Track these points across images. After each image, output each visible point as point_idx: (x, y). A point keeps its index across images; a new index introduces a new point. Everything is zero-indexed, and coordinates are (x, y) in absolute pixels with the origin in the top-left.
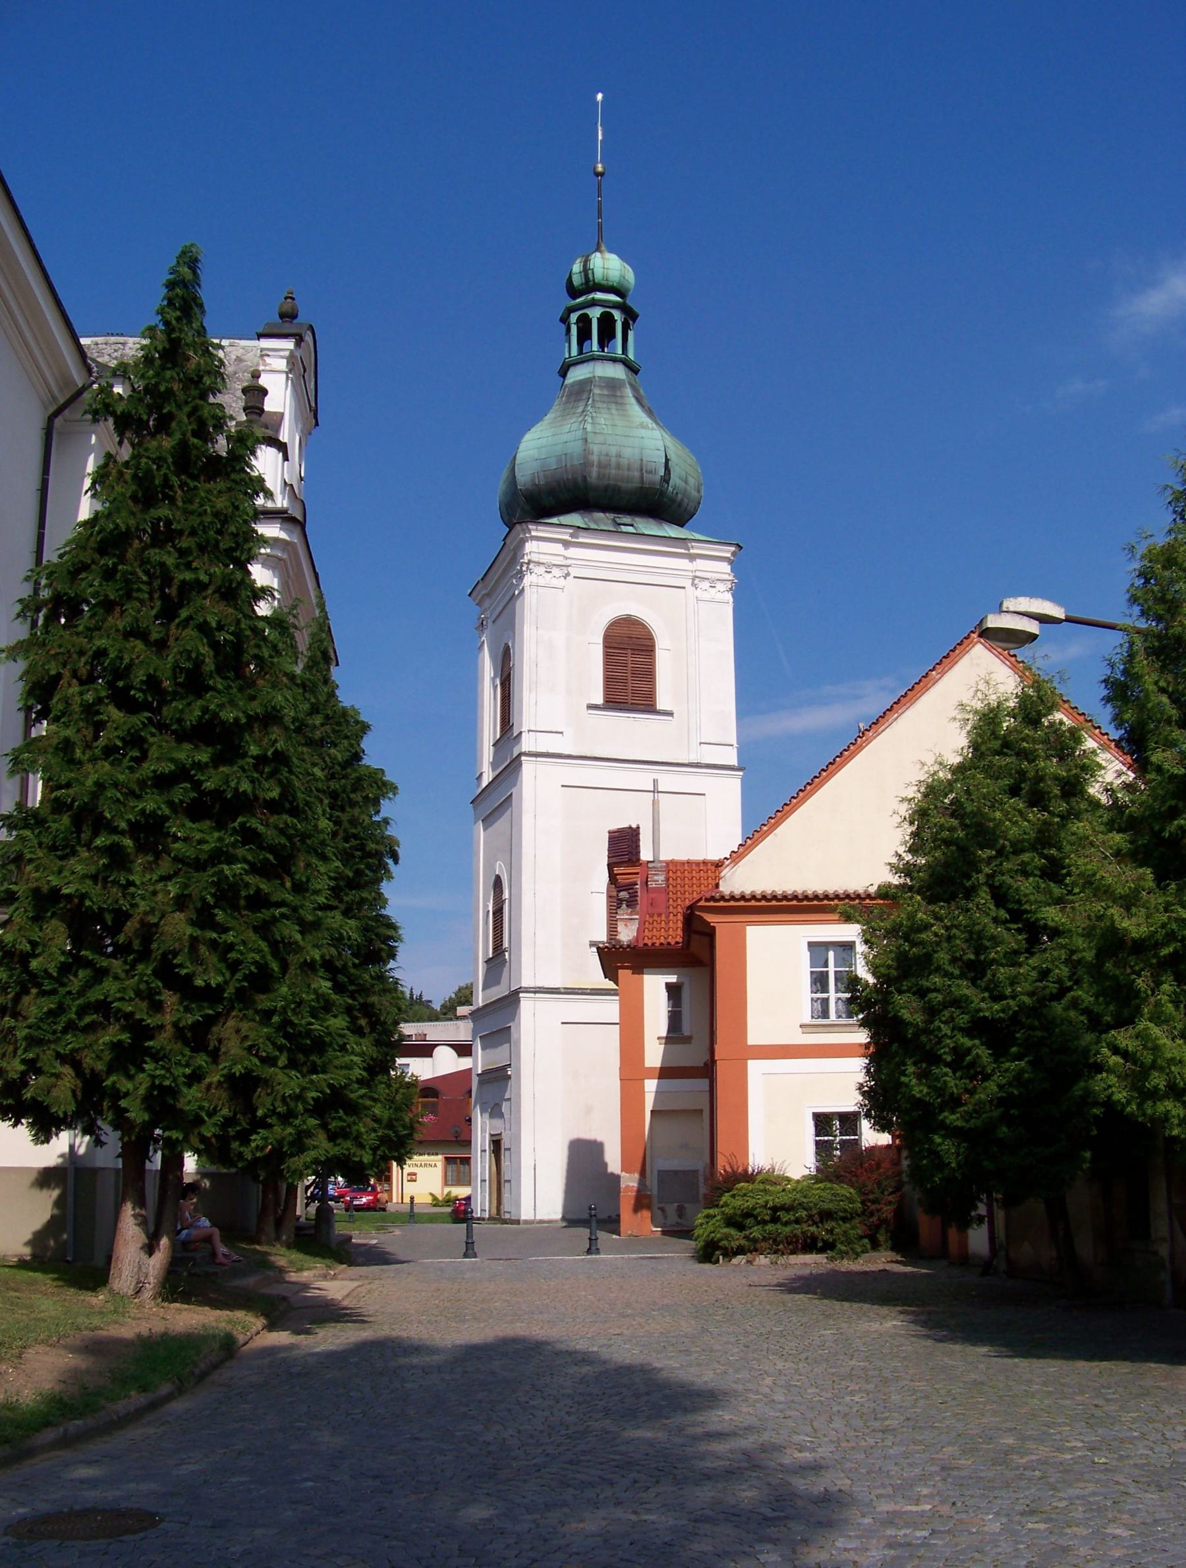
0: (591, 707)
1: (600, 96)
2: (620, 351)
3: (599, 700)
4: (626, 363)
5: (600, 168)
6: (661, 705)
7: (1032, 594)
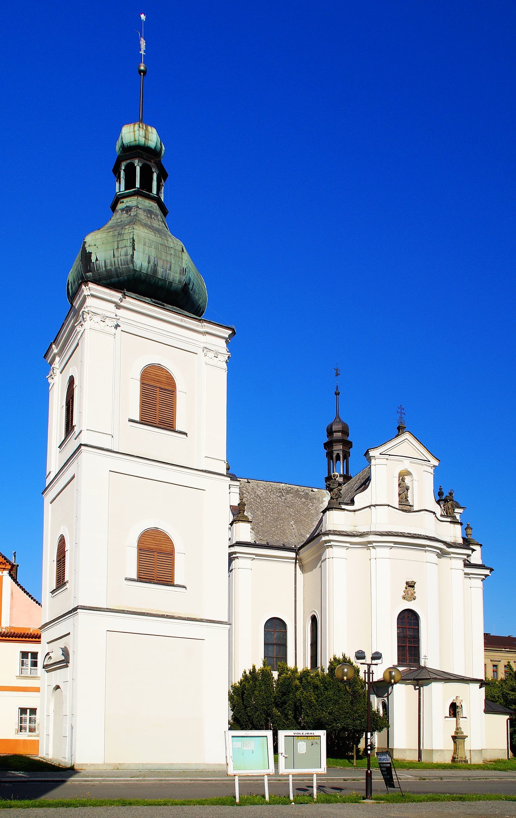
0: (131, 421)
1: (143, 17)
2: (154, 191)
3: (137, 418)
4: (157, 200)
5: (142, 68)
6: (178, 428)
7: (146, 46)
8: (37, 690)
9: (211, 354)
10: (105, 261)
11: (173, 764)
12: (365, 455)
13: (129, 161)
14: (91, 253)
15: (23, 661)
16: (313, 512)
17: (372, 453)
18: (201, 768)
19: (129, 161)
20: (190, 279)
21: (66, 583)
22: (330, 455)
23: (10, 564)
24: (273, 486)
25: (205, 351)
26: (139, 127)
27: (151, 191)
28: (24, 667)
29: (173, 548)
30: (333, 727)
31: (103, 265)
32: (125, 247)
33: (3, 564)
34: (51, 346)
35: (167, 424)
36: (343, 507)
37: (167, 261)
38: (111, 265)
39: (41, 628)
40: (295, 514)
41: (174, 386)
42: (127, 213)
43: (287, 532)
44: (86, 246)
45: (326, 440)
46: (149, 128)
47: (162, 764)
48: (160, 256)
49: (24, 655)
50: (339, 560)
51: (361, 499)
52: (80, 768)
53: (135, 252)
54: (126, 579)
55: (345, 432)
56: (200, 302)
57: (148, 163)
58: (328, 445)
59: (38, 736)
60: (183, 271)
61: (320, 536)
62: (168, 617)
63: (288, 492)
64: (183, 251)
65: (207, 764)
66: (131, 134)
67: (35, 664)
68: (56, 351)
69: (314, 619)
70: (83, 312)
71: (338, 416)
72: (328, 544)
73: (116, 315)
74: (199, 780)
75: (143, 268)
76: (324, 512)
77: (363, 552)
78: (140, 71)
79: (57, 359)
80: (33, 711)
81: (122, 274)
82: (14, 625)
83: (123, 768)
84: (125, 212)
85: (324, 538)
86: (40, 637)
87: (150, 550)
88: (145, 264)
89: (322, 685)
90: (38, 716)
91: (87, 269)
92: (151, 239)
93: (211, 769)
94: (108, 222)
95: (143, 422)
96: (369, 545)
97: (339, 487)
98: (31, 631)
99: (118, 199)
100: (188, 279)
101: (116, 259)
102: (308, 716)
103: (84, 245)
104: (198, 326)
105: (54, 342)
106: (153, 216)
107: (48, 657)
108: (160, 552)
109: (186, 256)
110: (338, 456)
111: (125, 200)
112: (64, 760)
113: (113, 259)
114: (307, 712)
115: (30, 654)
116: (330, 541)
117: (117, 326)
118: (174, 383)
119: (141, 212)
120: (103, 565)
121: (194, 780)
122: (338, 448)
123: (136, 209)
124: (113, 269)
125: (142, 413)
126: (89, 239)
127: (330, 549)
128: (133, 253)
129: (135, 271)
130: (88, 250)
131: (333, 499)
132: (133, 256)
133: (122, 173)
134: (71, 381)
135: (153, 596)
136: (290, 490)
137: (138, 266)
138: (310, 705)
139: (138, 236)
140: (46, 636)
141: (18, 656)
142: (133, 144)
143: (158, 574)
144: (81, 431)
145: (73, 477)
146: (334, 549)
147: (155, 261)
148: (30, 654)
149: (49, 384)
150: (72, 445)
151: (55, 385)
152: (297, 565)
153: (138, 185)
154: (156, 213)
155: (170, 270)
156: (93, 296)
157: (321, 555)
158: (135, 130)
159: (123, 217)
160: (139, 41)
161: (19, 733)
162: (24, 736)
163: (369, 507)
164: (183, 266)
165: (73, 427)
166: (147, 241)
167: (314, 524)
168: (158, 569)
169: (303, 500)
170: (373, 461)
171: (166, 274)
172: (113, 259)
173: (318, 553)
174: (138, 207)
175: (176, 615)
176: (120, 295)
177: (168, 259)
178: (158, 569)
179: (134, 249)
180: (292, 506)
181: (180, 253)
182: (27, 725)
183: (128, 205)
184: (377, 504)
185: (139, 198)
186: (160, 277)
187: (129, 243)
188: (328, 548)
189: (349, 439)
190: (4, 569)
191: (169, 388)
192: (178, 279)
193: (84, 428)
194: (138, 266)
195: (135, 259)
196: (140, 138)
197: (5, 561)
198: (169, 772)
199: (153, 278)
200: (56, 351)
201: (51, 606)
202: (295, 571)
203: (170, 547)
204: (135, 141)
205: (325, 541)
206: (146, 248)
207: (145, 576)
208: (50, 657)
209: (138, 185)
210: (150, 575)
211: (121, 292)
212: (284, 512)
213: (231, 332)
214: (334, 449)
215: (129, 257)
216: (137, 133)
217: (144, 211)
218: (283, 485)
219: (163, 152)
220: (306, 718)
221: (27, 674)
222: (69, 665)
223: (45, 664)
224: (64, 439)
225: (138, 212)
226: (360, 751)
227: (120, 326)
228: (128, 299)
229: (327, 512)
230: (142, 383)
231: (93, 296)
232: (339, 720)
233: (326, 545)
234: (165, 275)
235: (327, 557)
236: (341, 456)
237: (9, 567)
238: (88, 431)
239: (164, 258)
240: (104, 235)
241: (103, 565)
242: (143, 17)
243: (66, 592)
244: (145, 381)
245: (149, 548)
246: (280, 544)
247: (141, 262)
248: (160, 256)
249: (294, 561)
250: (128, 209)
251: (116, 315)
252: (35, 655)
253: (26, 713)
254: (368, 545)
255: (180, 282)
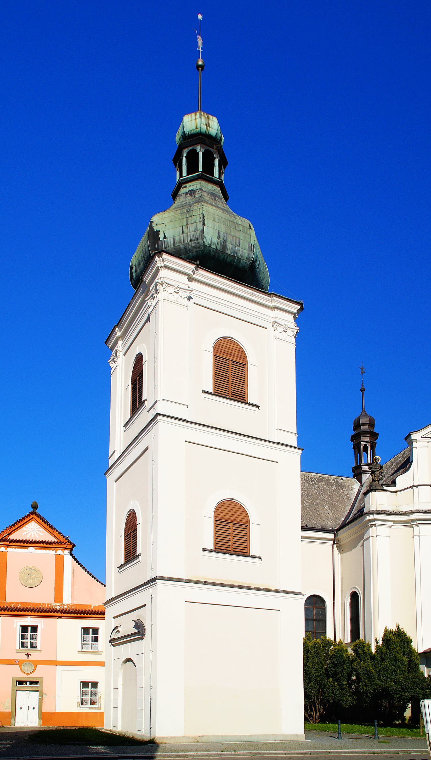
1: (200, 17)
2: (216, 174)
4: (219, 184)
5: (200, 63)
7: (203, 44)
8: (101, 664)
9: (280, 329)
10: (174, 238)
11: (251, 736)
12: (406, 439)
13: (191, 148)
14: (159, 231)
15: (83, 637)
16: (345, 497)
17: (413, 436)
18: (279, 739)
19: (191, 148)
20: (257, 257)
21: (138, 556)
22: (357, 447)
23: (71, 544)
24: (306, 476)
25: (275, 326)
26: (201, 115)
27: (213, 175)
28: (85, 642)
29: (248, 519)
30: (402, 696)
31: (172, 242)
32: (195, 222)
33: (65, 544)
34: (114, 328)
35: (240, 396)
36: (385, 488)
37: (236, 237)
38: (180, 242)
39: (105, 604)
40: (329, 499)
41: (245, 359)
42: (191, 195)
43: (323, 516)
44: (154, 225)
45: (353, 433)
46: (210, 117)
47: (241, 736)
48: (229, 231)
49: (86, 630)
50: (383, 539)
51: (402, 480)
52: (161, 741)
53: (205, 227)
54: (203, 550)
55: (371, 424)
56: (264, 282)
57: (210, 149)
58: (356, 438)
59: (99, 708)
60: (252, 248)
61: (364, 516)
62: (244, 587)
63: (320, 481)
64: (250, 228)
65: (285, 736)
66: (192, 122)
67: (95, 640)
68: (119, 334)
69: (354, 597)
70: (156, 283)
71: (364, 411)
72: (372, 523)
73: (189, 287)
74: (294, 753)
75: (213, 243)
76: (366, 494)
77: (406, 531)
78: (198, 67)
79: (120, 342)
80: (95, 685)
81: (190, 250)
82: (75, 602)
83: (203, 740)
84: (188, 195)
85: (369, 518)
86: (104, 614)
87: (226, 521)
88: (215, 240)
89: (379, 655)
90: (100, 689)
91: (155, 246)
92: (220, 215)
93: (288, 740)
94: (172, 205)
95: (216, 393)
96: (412, 523)
97: (381, 470)
98: (92, 608)
99: (180, 185)
100: (256, 256)
101: (185, 235)
102: (366, 686)
103: (151, 224)
104: (268, 300)
105: (117, 325)
106: (217, 199)
107: (116, 630)
108: (236, 523)
109: (253, 233)
110: (366, 447)
111: (188, 185)
112: (138, 733)
113: (182, 236)
114: (365, 682)
115: (91, 630)
116: (374, 520)
117: (190, 298)
118: (246, 357)
119: (205, 194)
120: (178, 537)
121: (289, 754)
122: (366, 440)
123: (200, 192)
124: (182, 246)
125: (216, 385)
126: (156, 219)
127: (374, 528)
128: (203, 228)
129: (205, 246)
130: (156, 228)
131: (375, 481)
132: (203, 231)
133: (184, 160)
134: (139, 359)
135: (229, 567)
136: (321, 479)
137: (208, 241)
138: (369, 675)
139: (207, 212)
140: (110, 611)
141: (80, 631)
142: (195, 131)
143: (234, 545)
144: (157, 401)
145: (147, 449)
146: (378, 527)
147: (224, 237)
148: (91, 630)
149: (110, 368)
150: (144, 416)
151: (118, 368)
152: (335, 545)
153: (200, 169)
154: (219, 196)
155: (239, 246)
156: (166, 267)
157: (363, 535)
158: (197, 117)
159: (187, 199)
160: (197, 38)
161: (81, 706)
162: (87, 709)
163: (411, 487)
164: (252, 243)
165: (142, 403)
166: (216, 217)
167: (347, 509)
168: (234, 540)
169: (335, 487)
170: (414, 444)
171: (235, 250)
172: (182, 236)
173: (360, 533)
174: (202, 190)
175: (252, 586)
176: (193, 267)
177: (237, 235)
178: (234, 540)
179: (204, 224)
180: (325, 492)
181: (248, 230)
182: (88, 698)
183: (191, 188)
184: (419, 484)
185: (202, 182)
186: (229, 253)
187: (199, 219)
188: (371, 527)
189: (375, 430)
190: (66, 548)
191: (241, 361)
192: (246, 255)
193: (159, 398)
194: (208, 241)
195: (205, 234)
196: (202, 125)
197: (67, 541)
198: (252, 744)
199: (223, 254)
200: (119, 334)
201: (116, 581)
202: (333, 551)
203: (245, 518)
204: (197, 128)
205: (369, 520)
206: (216, 224)
207: (221, 547)
208: (118, 631)
209: (200, 169)
210: (226, 546)
211: (194, 264)
212: (318, 498)
213: (299, 307)
214: (362, 440)
215: (199, 232)
216: (199, 120)
217: (208, 193)
218: (315, 474)
219: (223, 141)
220: (365, 688)
221: (88, 648)
222: (144, 637)
223: (112, 638)
224: (129, 417)
225: (203, 194)
226: (405, 719)
227: (192, 299)
228: (201, 271)
229: (370, 493)
230: (215, 356)
231: (166, 267)
232: (407, 689)
233: (371, 524)
234: (234, 252)
235: (371, 536)
236: (369, 446)
237: (70, 547)
238: (164, 401)
239: (233, 233)
240: (172, 214)
241: (178, 537)
242: (200, 17)
243: (138, 565)
244: (218, 354)
245: (225, 519)
246: (319, 526)
247: (211, 237)
248: (229, 231)
249: (332, 542)
250: (192, 193)
251: (189, 287)
252: (96, 631)
253: (87, 687)
254: (411, 523)
255: (248, 258)
